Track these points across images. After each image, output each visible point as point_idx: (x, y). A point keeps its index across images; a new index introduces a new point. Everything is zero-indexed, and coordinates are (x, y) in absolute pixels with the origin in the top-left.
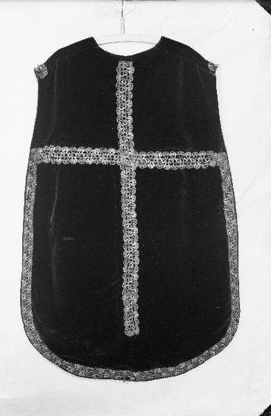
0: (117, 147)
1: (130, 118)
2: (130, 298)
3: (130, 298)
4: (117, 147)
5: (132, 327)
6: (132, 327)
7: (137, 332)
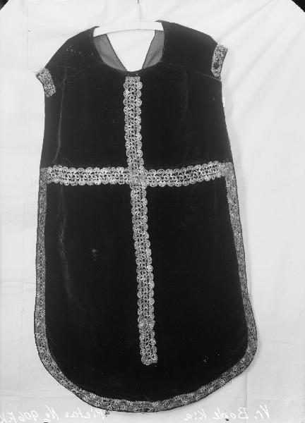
0: (125, 166)
1: (139, 136)
2: (146, 323)
3: (146, 323)
4: (125, 166)
5: (149, 355)
6: (149, 355)
7: (155, 359)
